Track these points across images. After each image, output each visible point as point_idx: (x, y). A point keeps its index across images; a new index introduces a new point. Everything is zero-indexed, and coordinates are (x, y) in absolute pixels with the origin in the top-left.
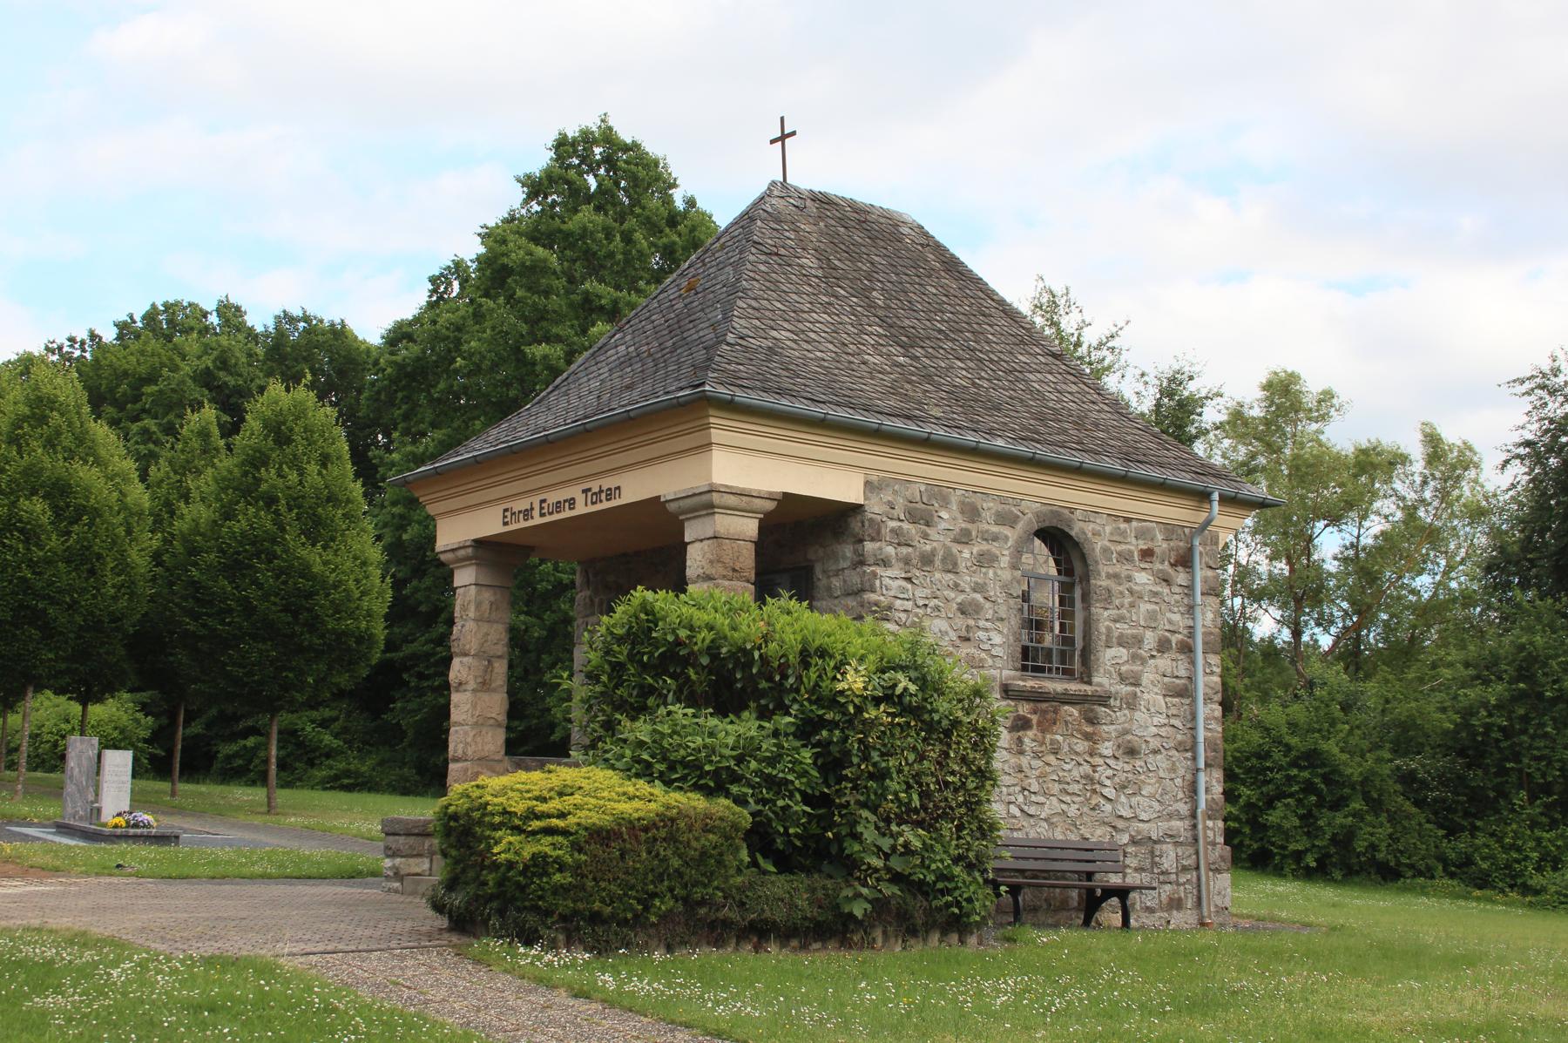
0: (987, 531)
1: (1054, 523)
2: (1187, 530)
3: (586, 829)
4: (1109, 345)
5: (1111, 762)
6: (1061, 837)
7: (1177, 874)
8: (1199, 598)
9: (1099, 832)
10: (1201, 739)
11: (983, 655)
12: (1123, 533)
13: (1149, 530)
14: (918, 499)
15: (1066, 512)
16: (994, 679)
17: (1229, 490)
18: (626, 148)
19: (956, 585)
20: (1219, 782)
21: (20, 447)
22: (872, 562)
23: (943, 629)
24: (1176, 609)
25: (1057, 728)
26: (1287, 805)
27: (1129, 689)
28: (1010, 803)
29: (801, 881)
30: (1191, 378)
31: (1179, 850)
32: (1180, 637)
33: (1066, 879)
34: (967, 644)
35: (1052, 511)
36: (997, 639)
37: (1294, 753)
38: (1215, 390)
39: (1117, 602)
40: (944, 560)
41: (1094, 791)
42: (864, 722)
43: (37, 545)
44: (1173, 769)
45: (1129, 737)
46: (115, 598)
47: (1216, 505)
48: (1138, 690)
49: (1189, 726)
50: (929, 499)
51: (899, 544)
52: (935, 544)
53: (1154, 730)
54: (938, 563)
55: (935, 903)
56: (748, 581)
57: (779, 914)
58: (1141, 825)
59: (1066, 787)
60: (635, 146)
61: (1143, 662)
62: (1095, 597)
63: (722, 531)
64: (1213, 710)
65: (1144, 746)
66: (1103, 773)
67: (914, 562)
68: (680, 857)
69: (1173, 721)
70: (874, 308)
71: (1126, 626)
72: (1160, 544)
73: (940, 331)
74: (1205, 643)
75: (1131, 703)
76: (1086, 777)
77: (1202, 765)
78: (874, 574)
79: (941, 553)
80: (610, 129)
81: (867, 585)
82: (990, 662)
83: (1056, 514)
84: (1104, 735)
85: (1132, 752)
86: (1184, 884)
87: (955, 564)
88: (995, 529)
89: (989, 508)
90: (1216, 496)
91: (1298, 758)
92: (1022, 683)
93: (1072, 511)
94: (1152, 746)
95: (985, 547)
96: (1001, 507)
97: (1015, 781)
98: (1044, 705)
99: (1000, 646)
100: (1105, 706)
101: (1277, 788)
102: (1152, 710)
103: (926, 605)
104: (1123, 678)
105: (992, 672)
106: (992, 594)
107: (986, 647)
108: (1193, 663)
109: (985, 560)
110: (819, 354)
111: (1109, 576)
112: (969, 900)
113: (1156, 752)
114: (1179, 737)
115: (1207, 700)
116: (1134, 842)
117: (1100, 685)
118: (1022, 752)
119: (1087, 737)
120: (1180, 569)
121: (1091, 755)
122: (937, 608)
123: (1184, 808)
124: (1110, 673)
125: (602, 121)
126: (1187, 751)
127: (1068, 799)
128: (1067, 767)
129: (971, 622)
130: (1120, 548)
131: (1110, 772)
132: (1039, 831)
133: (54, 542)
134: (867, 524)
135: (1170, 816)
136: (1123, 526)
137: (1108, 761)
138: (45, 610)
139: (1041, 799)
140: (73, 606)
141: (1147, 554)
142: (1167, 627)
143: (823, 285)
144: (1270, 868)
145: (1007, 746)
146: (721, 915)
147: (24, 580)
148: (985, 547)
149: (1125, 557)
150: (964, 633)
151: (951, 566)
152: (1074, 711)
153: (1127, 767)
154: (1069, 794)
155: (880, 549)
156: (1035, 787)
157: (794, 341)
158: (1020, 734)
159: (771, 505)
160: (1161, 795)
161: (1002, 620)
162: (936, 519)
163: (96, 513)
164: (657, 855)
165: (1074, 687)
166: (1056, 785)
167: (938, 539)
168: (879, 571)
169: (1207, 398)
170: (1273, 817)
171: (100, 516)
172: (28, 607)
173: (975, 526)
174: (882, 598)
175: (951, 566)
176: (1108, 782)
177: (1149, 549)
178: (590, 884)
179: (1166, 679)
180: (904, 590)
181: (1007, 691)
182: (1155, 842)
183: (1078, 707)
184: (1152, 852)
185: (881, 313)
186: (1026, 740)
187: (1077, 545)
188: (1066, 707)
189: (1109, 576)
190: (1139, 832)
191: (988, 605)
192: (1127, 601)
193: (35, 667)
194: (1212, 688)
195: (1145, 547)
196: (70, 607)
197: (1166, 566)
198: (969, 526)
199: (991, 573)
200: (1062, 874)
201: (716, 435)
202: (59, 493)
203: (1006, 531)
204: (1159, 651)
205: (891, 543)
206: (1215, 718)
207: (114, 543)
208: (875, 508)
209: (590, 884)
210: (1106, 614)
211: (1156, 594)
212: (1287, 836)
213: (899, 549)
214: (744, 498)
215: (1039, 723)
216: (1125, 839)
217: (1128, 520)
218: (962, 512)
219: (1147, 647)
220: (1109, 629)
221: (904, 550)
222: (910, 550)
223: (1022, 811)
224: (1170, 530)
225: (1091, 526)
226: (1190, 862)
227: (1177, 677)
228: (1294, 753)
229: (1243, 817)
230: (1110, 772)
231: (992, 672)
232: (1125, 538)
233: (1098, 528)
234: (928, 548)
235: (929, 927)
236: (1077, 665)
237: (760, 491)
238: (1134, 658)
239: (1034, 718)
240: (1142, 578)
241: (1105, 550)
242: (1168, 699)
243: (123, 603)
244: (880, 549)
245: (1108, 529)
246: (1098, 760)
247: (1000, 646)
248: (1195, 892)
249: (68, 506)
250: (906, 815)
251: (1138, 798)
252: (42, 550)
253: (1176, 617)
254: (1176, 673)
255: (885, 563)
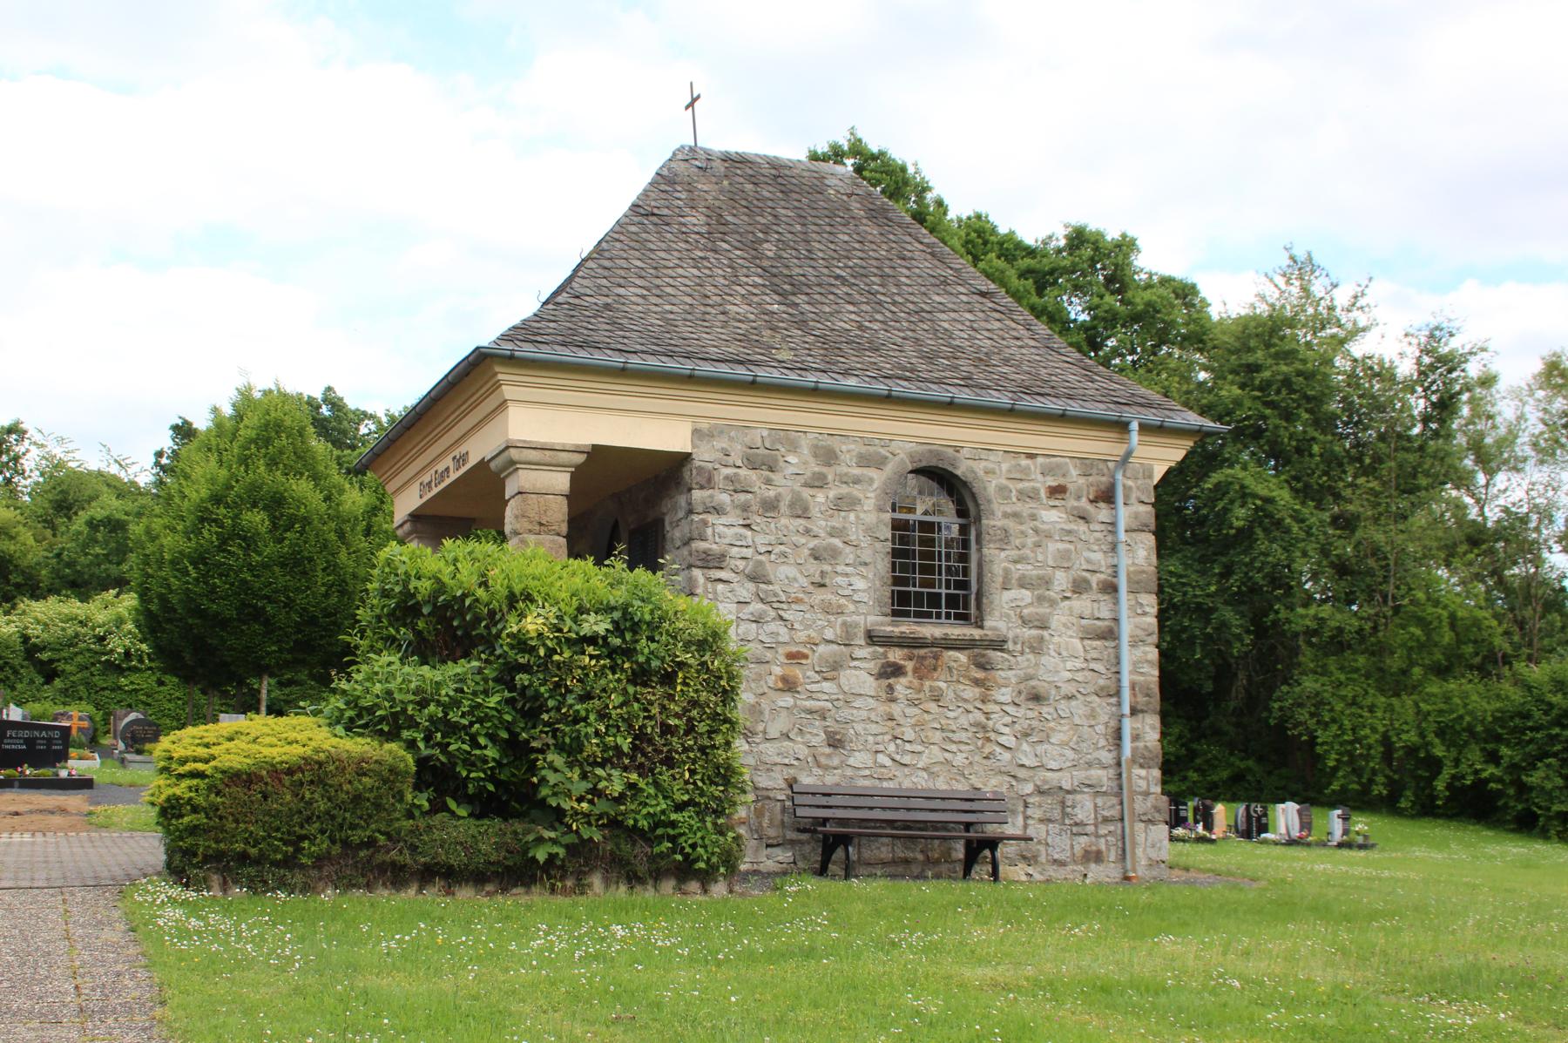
0: (846, 474)
1: (934, 463)
2: (1110, 464)
3: (223, 772)
4: (1358, 305)
5: (1009, 709)
6: (944, 787)
7: (1096, 826)
8: (1122, 536)
9: (994, 782)
10: (1126, 683)
11: (843, 601)
12: (1026, 470)
13: (1058, 466)
14: (759, 444)
15: (950, 450)
16: (857, 625)
17: (1152, 417)
18: (874, 157)
19: (808, 531)
20: (1153, 728)
21: (247, 466)
22: (700, 510)
23: (791, 575)
24: (1096, 548)
25: (942, 674)
26: (1548, 766)
27: (1034, 632)
28: (877, 752)
29: (494, 825)
30: (1451, 335)
31: (1100, 801)
32: (1102, 577)
33: (949, 831)
34: (823, 589)
35: (930, 451)
36: (860, 584)
37: (1555, 712)
38: (1480, 345)
39: (1017, 542)
40: (792, 505)
41: (988, 740)
42: (558, 665)
43: (255, 551)
44: (1092, 715)
45: (1033, 683)
46: (326, 595)
47: (1135, 437)
48: (1045, 633)
49: (1114, 670)
50: (773, 443)
51: (735, 491)
52: (780, 490)
53: (1069, 675)
54: (783, 507)
55: (657, 850)
56: (558, 535)
57: (457, 859)
58: (1049, 774)
59: (950, 735)
60: (882, 154)
61: (1053, 603)
62: (987, 537)
63: (527, 487)
64: (1145, 653)
65: (1053, 692)
66: (998, 721)
67: (754, 508)
68: (330, 799)
69: (1093, 665)
70: (760, 259)
71: (1030, 567)
72: (1074, 478)
73: (838, 277)
74: (1129, 580)
75: (1037, 647)
76: (977, 724)
77: (1127, 710)
78: (705, 523)
79: (789, 498)
80: (860, 140)
81: (695, 534)
82: (852, 607)
83: (938, 455)
84: (1001, 681)
85: (1036, 698)
86: (1105, 836)
87: (806, 509)
88: (857, 471)
89: (848, 451)
90: (1135, 426)
91: (1561, 716)
92: (889, 629)
93: (957, 449)
94: (1063, 691)
95: (844, 490)
96: (864, 449)
97: (885, 730)
98: (922, 652)
99: (864, 591)
100: (1002, 650)
101: (1539, 749)
102: (1065, 654)
103: (770, 552)
104: (1025, 622)
105: (855, 618)
106: (853, 538)
107: (846, 592)
108: (1116, 602)
109: (842, 504)
110: (668, 307)
111: (1006, 515)
112: (694, 846)
113: (1070, 698)
114: (1102, 682)
115: (1134, 643)
116: (1040, 792)
117: (994, 629)
118: (893, 700)
119: (977, 682)
120: (1102, 505)
121: (983, 702)
122: (784, 555)
123: (1107, 757)
124: (1008, 616)
125: (852, 134)
126: (1111, 696)
127: (953, 747)
128: (951, 715)
129: (827, 568)
130: (1020, 485)
131: (1008, 720)
132: (920, 781)
133: (270, 549)
134: (694, 472)
135: (1089, 765)
136: (1025, 462)
137: (1005, 708)
138: (264, 608)
139: (919, 748)
140: (289, 604)
141: (1057, 491)
142: (1084, 567)
143: (703, 241)
144: (1537, 830)
145: (873, 694)
146: (387, 858)
147: (244, 581)
148: (844, 490)
149: (1024, 496)
150: (817, 579)
151: (801, 510)
152: (962, 657)
153: (1030, 714)
154: (954, 742)
155: (711, 496)
156: (910, 734)
157: (643, 297)
158: (891, 681)
159: (581, 458)
160: (1078, 743)
161: (866, 564)
162: (782, 464)
163: (306, 521)
164: (303, 797)
165: (957, 631)
166: (938, 733)
167: (784, 485)
168: (711, 518)
169: (1471, 353)
170: (1534, 778)
171: (309, 523)
172: (250, 605)
173: (832, 469)
174: (714, 546)
175: (801, 510)
176: (1006, 730)
177: (1059, 486)
178: (230, 825)
179: (1084, 622)
180: (741, 537)
181: (872, 638)
182: (1068, 792)
183: (966, 652)
184: (1063, 802)
185: (766, 263)
186: (898, 687)
187: (965, 484)
188: (951, 653)
189: (1006, 515)
190: (1045, 782)
191: (848, 549)
192: (1030, 541)
193: (263, 658)
194: (1144, 630)
195: (1054, 484)
196: (286, 605)
197: (1084, 503)
198: (824, 470)
199: (852, 516)
200: (944, 825)
201: (508, 391)
202: (275, 503)
203: (872, 473)
204: (1074, 592)
205: (725, 491)
206: (1148, 661)
207: (325, 546)
208: (704, 455)
209: (230, 825)
210: (1003, 554)
211: (1069, 532)
212: (1549, 796)
213: (736, 495)
214: (547, 452)
215: (915, 670)
216: (1028, 788)
217: (1031, 456)
218: (815, 456)
219: (1058, 589)
220: (1007, 571)
221: (742, 497)
222: (749, 496)
223: (893, 760)
224: (1087, 465)
225: (983, 464)
226: (1115, 812)
227: (1098, 619)
228: (1555, 712)
229: (1507, 778)
230: (1008, 720)
231: (855, 618)
232: (1027, 475)
233: (991, 466)
234: (772, 493)
235: (657, 876)
236: (973, 610)
237: (564, 444)
238: (1040, 599)
239: (909, 666)
240: (1052, 517)
241: (1002, 489)
242: (1087, 642)
243: (334, 600)
244: (711, 496)
245: (1005, 467)
246: (990, 707)
247: (864, 591)
248: (1120, 844)
249: (282, 515)
250: (612, 758)
251: (1045, 746)
252: (260, 555)
253: (1097, 557)
254: (1097, 615)
255: (718, 510)
